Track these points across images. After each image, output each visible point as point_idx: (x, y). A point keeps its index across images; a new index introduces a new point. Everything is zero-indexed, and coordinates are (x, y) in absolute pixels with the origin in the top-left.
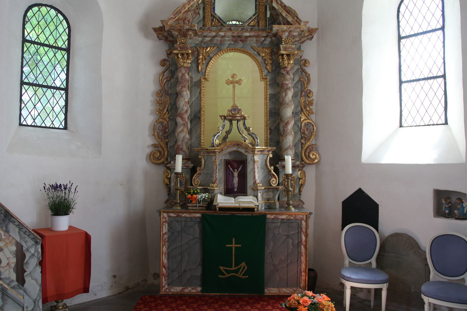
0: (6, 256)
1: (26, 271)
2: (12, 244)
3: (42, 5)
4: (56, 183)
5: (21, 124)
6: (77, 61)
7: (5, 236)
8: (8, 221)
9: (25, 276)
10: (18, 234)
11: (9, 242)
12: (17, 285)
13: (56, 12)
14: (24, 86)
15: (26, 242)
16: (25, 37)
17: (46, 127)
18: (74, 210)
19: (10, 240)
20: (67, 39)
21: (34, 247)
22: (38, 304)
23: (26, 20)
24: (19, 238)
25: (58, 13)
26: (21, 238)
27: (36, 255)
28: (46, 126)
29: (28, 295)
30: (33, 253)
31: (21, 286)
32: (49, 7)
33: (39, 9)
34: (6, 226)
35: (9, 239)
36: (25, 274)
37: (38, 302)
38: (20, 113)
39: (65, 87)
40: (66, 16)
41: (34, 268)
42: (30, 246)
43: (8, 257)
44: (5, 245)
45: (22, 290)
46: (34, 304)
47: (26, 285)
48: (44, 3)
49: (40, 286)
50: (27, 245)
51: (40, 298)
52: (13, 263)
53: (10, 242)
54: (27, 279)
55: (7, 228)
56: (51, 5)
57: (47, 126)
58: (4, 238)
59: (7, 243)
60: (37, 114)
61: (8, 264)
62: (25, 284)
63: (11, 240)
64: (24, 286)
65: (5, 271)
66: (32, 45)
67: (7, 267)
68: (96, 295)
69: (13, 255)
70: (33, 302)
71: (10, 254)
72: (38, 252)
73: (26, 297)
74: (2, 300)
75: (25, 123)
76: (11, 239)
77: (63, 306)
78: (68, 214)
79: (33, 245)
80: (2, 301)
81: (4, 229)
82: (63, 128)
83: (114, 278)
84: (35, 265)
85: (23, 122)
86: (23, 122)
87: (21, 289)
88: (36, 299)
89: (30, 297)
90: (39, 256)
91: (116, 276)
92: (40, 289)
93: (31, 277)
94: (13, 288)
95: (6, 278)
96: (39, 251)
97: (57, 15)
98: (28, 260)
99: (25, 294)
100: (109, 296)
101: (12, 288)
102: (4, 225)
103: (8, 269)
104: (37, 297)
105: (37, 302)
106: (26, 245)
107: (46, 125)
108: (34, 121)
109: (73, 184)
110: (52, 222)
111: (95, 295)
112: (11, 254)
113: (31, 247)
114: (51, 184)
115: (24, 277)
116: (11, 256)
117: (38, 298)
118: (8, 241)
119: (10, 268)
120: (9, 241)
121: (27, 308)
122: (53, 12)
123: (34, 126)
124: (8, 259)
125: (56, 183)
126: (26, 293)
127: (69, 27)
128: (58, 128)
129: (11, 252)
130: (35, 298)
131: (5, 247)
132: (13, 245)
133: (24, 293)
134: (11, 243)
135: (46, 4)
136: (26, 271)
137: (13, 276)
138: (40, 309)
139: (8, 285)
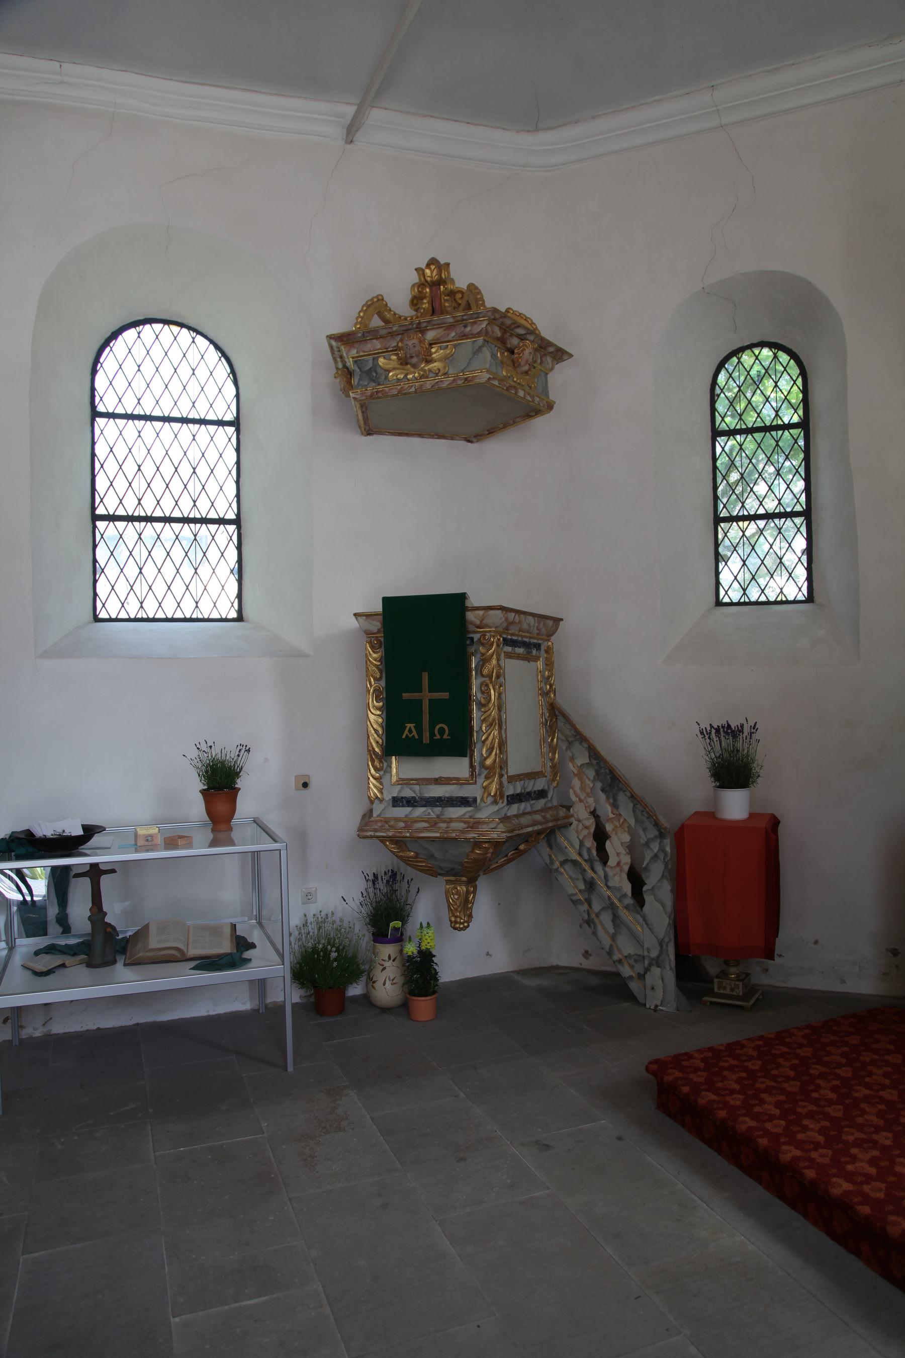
0: (615, 850)
1: (646, 884)
2: (623, 830)
3: (742, 349)
4: (727, 721)
5: (719, 603)
6: (821, 445)
7: (614, 815)
8: (616, 788)
9: (644, 891)
10: (632, 813)
11: (619, 826)
12: (633, 904)
13: (773, 350)
14: (722, 525)
15: (645, 830)
16: (717, 427)
17: (768, 603)
18: (759, 780)
19: (621, 823)
20: (802, 401)
21: (659, 840)
22: (667, 951)
23: (716, 393)
24: (634, 821)
25: (777, 352)
26: (637, 821)
27: (662, 856)
28: (768, 600)
29: (650, 929)
30: (656, 851)
31: (638, 908)
32: (757, 347)
33: (739, 359)
34: (613, 797)
35: (619, 820)
36: (644, 889)
37: (667, 946)
38: (716, 580)
39: (804, 507)
40: (795, 350)
41: (658, 881)
42: (652, 838)
43: (619, 852)
44: (613, 830)
45: (639, 916)
46: (659, 948)
47: (646, 908)
48: (746, 344)
49: (669, 917)
50: (646, 835)
51: (670, 941)
52: (626, 864)
53: (620, 826)
54: (648, 898)
55: (615, 800)
56: (760, 341)
57: (771, 600)
58: (613, 818)
59: (616, 827)
60: (748, 576)
61: (618, 864)
62: (645, 906)
63: (623, 822)
64: (643, 909)
65: (614, 875)
66: (768, 433)
67: (618, 869)
68: (845, 982)
69: (625, 850)
70: (658, 944)
71: (621, 847)
72: (664, 851)
73: (647, 931)
74: (613, 925)
75: (726, 600)
76: (622, 820)
77: (738, 975)
78: (748, 787)
79: (656, 837)
80: (613, 927)
81: (611, 801)
82: (804, 599)
83: (891, 955)
84: (660, 876)
85: (723, 598)
86: (723, 598)
87: (638, 913)
88: (663, 939)
89: (653, 933)
90: (666, 861)
91: (900, 953)
92: (669, 924)
93: (654, 896)
94: (627, 907)
95: (615, 888)
96: (666, 851)
97: (775, 356)
98: (648, 864)
99: (645, 926)
100: (878, 996)
101: (626, 908)
102: (611, 794)
103: (619, 872)
104: (664, 937)
105: (664, 947)
106: (644, 837)
107: (769, 598)
108: (744, 594)
109: (757, 724)
110: (715, 800)
111: (843, 981)
112: (623, 847)
113: (653, 840)
114: (705, 725)
115: (643, 893)
116: (622, 850)
117: (667, 939)
118: (617, 824)
119: (621, 871)
120: (619, 824)
121: (648, 952)
122: (766, 353)
123: (745, 604)
124: (618, 854)
125: (727, 721)
126: (647, 924)
127: (803, 373)
128: (795, 602)
129: (622, 844)
130: (661, 936)
131: (614, 833)
132: (625, 831)
133: (644, 922)
134: (622, 828)
135: (749, 343)
136: (646, 884)
137: (627, 888)
138: (670, 960)
139: (620, 900)
